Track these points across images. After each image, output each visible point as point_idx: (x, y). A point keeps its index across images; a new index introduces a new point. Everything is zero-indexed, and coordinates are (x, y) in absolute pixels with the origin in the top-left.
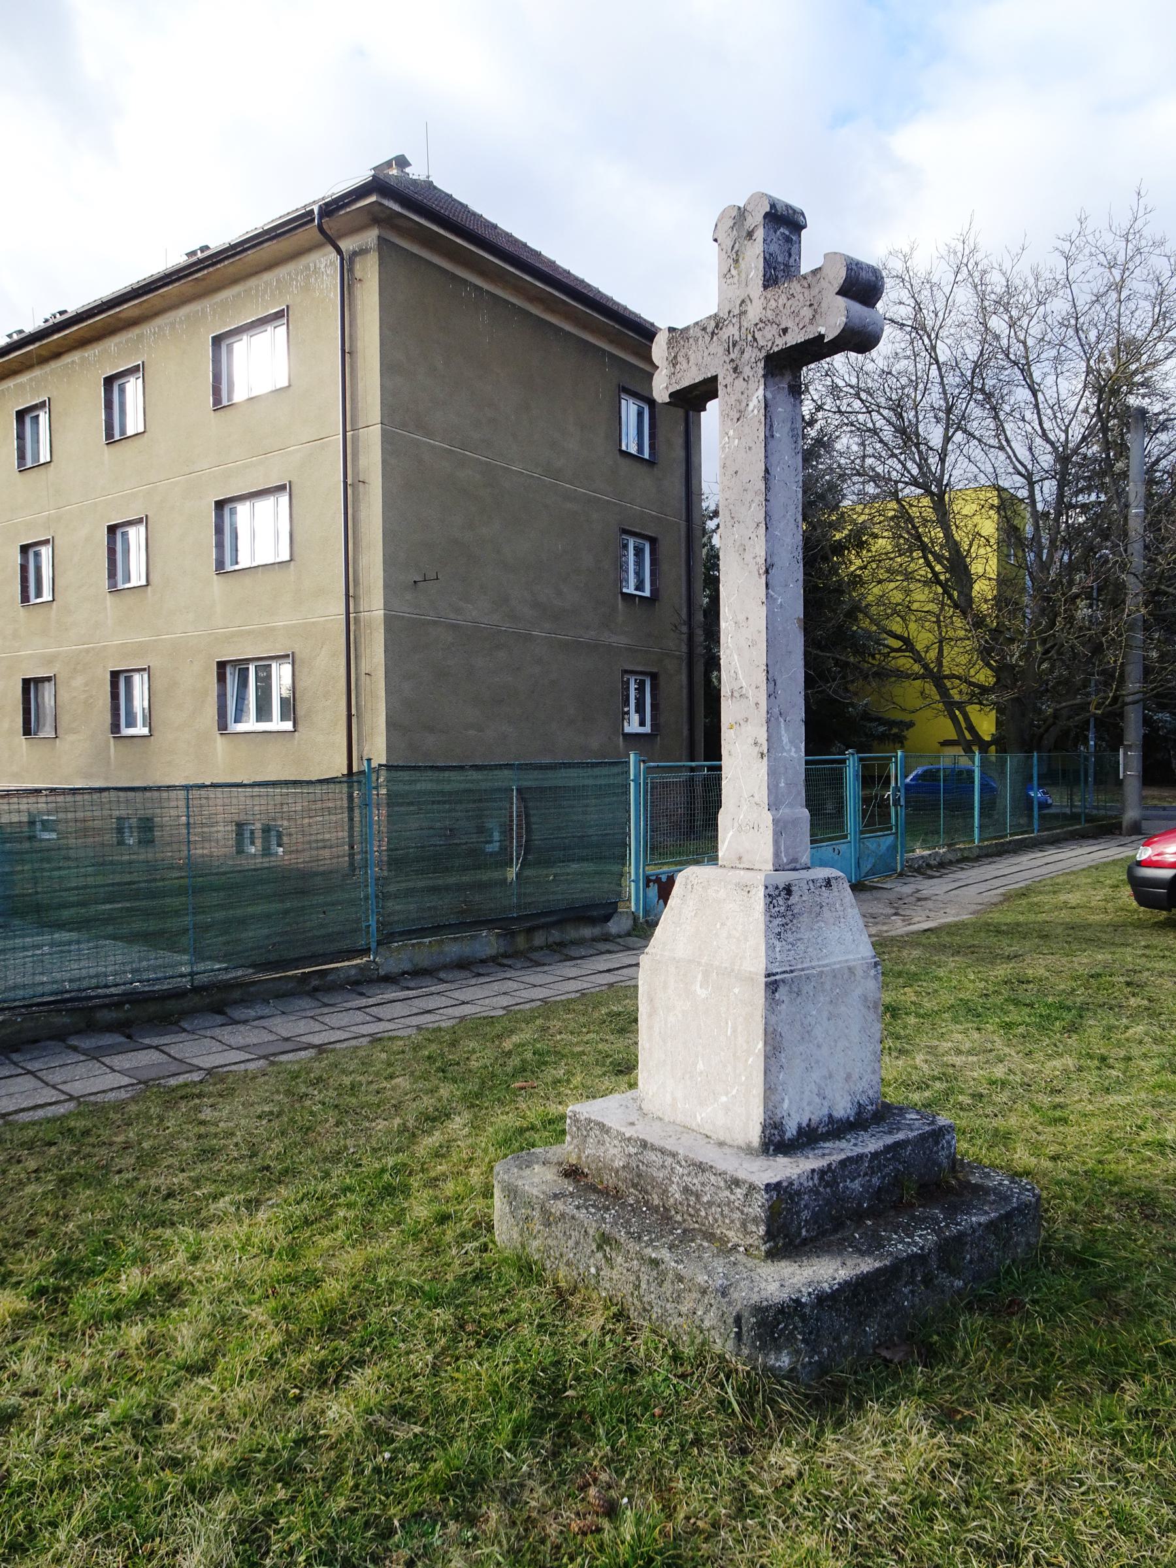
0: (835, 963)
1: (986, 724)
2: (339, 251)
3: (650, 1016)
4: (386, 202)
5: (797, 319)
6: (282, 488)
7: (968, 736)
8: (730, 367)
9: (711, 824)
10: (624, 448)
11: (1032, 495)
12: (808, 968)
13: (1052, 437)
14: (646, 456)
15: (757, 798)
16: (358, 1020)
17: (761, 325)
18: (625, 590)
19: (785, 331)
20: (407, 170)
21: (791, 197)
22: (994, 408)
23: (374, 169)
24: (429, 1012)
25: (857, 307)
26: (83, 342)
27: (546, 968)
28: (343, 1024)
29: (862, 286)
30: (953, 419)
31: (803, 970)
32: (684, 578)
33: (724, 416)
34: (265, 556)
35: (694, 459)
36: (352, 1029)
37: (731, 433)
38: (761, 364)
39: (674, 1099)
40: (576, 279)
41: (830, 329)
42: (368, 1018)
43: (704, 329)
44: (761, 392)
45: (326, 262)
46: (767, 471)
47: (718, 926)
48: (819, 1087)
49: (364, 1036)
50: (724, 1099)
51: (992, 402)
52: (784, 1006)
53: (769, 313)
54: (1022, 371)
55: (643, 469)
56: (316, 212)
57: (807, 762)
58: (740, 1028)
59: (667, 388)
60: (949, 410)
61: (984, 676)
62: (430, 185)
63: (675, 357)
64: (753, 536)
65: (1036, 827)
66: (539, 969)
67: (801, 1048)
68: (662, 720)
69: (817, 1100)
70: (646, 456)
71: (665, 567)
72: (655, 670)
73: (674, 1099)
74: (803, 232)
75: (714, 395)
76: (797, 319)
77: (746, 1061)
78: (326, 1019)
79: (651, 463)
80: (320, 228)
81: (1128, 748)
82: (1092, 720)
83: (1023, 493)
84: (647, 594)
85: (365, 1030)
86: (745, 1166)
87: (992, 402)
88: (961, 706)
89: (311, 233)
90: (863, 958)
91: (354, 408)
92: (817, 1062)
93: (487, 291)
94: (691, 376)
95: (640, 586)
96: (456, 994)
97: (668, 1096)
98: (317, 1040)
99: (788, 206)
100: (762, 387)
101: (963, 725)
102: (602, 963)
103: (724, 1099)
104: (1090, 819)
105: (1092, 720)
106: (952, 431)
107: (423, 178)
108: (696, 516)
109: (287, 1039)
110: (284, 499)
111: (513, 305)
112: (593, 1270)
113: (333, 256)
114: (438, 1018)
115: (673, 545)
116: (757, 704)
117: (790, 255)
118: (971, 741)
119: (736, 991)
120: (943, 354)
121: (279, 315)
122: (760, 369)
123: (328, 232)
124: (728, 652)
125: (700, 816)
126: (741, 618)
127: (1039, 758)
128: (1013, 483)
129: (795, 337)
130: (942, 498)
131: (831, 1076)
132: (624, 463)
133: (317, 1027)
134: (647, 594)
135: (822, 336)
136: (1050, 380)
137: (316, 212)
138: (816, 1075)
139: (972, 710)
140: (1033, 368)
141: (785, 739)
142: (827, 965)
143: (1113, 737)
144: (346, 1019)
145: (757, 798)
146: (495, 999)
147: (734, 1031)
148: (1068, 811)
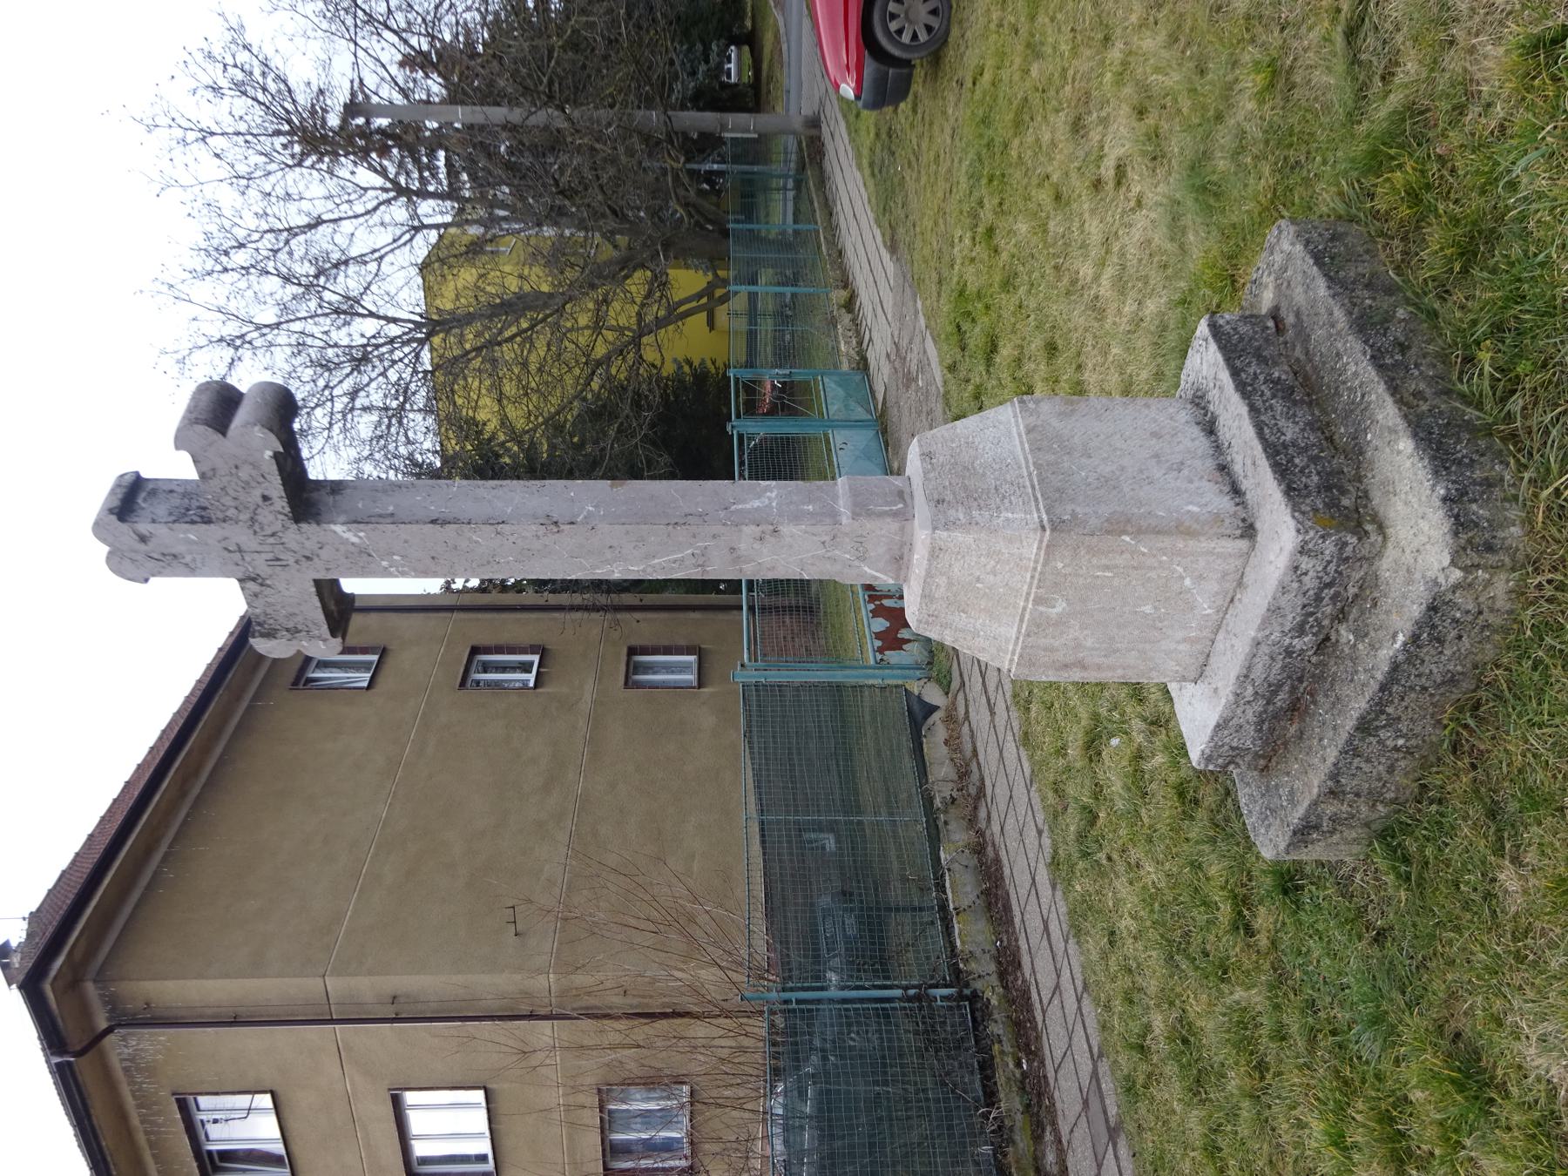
0: (1023, 449)
1: (687, 281)
2: (109, 1030)
3: (1084, 667)
4: (53, 973)
5: (253, 484)
6: (397, 1102)
7: (704, 300)
8: (304, 563)
9: (801, 586)
10: (365, 684)
11: (437, 226)
12: (1031, 481)
13: (370, 206)
14: (375, 658)
16: (1059, 1013)
17: (257, 527)
18: (531, 684)
19: (265, 498)
20: (14, 944)
21: (97, 493)
22: (336, 266)
23: (10, 984)
24: (1046, 928)
25: (242, 415)
26: (96, 1137)
27: (988, 783)
28: (1063, 1032)
29: (219, 406)
30: (348, 309)
31: (1033, 487)
32: (519, 615)
33: (364, 572)
34: (478, 1120)
35: (379, 603)
36: (1070, 1022)
37: (385, 563)
38: (304, 526)
39: (1184, 640)
40: (160, 738)
41: (267, 447)
42: (1056, 1001)
43: (256, 595)
44: (338, 528)
45: (118, 1048)
46: (433, 522)
48: (1171, 469)
49: (1080, 1008)
50: (1188, 582)
51: (328, 268)
52: (1078, 510)
53: (242, 517)
54: (296, 235)
55: (390, 661)
56: (58, 1060)
57: (742, 477)
58: (1104, 561)
59: (325, 640)
60: (337, 311)
61: (637, 283)
62: (34, 918)
63: (288, 630)
64: (512, 539)
65: (811, 227)
66: (989, 791)
67: (1126, 490)
68: (682, 642)
69: (1186, 472)
70: (375, 658)
71: (505, 638)
72: (625, 651)
73: (1184, 640)
74: (144, 475)
75: (335, 583)
76: (253, 484)
78: (1058, 1054)
79: (384, 653)
80: (78, 1054)
81: (724, 127)
82: (688, 166)
83: (433, 236)
84: (536, 658)
85: (1071, 1004)
86: (1272, 558)
87: (328, 268)
88: (672, 308)
89: (85, 1068)
90: (1015, 416)
91: (147, 851)
92: (1141, 471)
93: (170, 846)
94: (314, 611)
95: (526, 667)
96: (1023, 892)
97: (1181, 647)
98: (1086, 1067)
99: (113, 492)
100: (333, 527)
101: (694, 304)
102: (980, 717)
103: (1188, 582)
104: (802, 167)
105: (688, 166)
106: (361, 311)
107: (25, 925)
108: (450, 600)
109: (1086, 1103)
110: (410, 1097)
111: (188, 815)
112: (1401, 742)
113: (111, 1039)
114: (1053, 916)
115: (483, 629)
116: (714, 536)
117: (171, 491)
118: (710, 300)
119: (1060, 565)
120: (269, 316)
121: (183, 1106)
122: (308, 528)
123: (85, 1043)
124: (649, 570)
125: (791, 600)
126: (609, 554)
128: (422, 246)
129: (275, 487)
130: (437, 323)
131: (1156, 456)
132: (384, 683)
133: (1068, 1065)
134: (536, 658)
135: (276, 456)
136: (305, 205)
137: (58, 1060)
138: (1157, 473)
139: (677, 296)
141: (757, 504)
142: (1026, 459)
143: (707, 143)
144: (1058, 1029)
146: (1028, 846)
147: (1107, 568)
148: (791, 194)
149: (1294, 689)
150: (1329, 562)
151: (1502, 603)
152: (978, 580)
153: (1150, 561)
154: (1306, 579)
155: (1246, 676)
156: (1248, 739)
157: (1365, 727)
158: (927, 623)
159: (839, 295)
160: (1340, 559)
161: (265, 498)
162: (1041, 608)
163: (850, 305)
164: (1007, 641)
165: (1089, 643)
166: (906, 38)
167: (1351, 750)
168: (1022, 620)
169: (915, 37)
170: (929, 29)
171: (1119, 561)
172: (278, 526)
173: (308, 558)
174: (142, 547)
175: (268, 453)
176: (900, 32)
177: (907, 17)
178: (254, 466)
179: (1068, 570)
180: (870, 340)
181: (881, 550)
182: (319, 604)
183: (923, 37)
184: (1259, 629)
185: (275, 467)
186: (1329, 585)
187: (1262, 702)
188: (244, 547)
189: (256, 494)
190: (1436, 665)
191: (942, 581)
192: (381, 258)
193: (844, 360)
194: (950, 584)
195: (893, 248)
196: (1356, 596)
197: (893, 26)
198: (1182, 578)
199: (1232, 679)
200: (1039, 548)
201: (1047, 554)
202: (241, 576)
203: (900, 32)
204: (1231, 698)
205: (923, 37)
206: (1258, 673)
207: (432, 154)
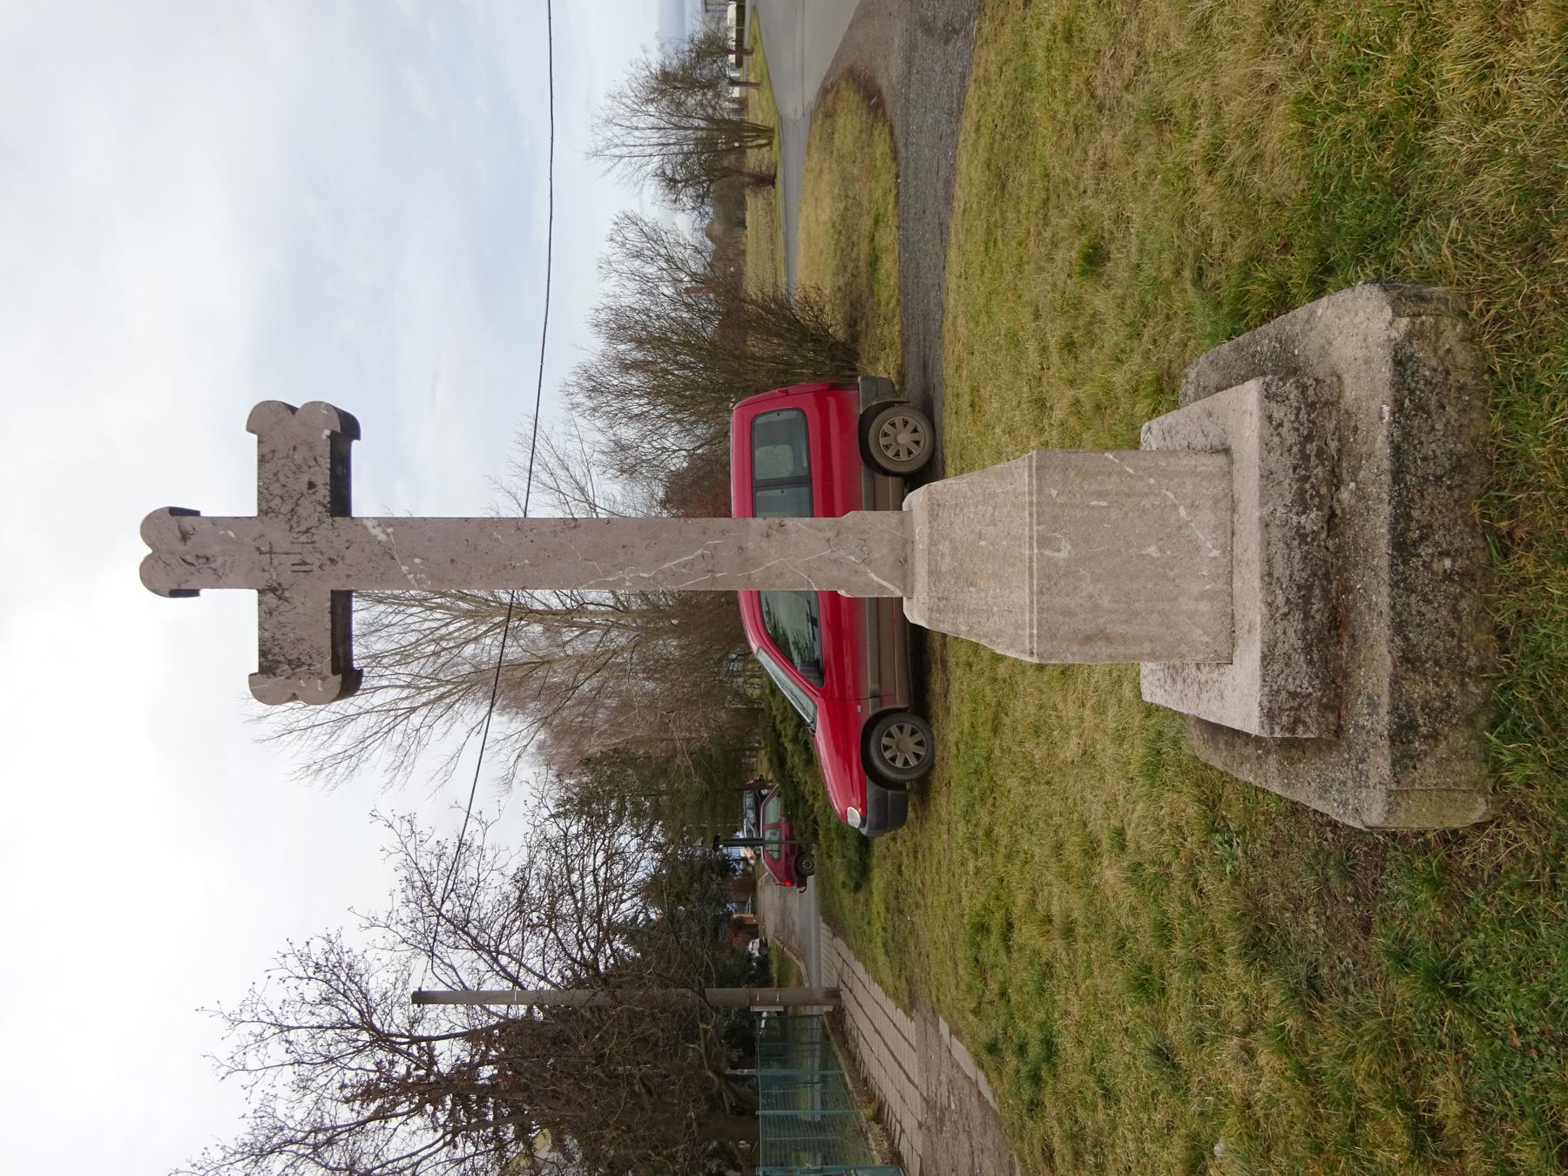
5: (305, 468)
8: (328, 568)
15: (831, 534)
19: (311, 485)
37: (405, 568)
47: (983, 543)
50: (1183, 512)
58: (1095, 487)
64: (531, 537)
65: (836, 1072)
76: (305, 468)
77: (1131, 476)
81: (753, 1002)
103: (1183, 512)
119: (1054, 493)
127: (764, 1108)
135: (333, 434)
140: (340, 1122)
145: (831, 534)
147: (1100, 495)
149: (1326, 592)
150: (1299, 409)
151: (1462, 356)
152: (980, 536)
153: (1140, 485)
154: (1284, 431)
155: (1270, 575)
156: (1302, 679)
157: (1402, 547)
158: (939, 611)
159: (866, 1112)
160: (1307, 405)
161: (311, 485)
162: (1047, 552)
163: (878, 1117)
164: (1022, 609)
165: (1105, 602)
166: (899, 764)
167: (1401, 584)
168: (1031, 576)
169: (906, 762)
170: (917, 756)
171: (1111, 484)
172: (314, 521)
173: (332, 561)
174: (181, 547)
175: (327, 432)
176: (893, 759)
177: (898, 749)
178: (311, 448)
179: (1062, 500)
180: (902, 1131)
181: (885, 550)
182: (329, 626)
183: (913, 762)
184: (1263, 504)
185: (328, 449)
186: (1308, 438)
187: (1299, 615)
188: (276, 549)
189: (305, 479)
190: (1436, 446)
191: (945, 547)
194: (954, 550)
196: (1339, 451)
197: (888, 755)
198: (1175, 507)
199: (1257, 584)
200: (1030, 476)
201: (1039, 479)
202: (262, 585)
203: (893, 759)
204: (1265, 610)
205: (913, 762)
206: (1280, 569)
207: (481, 1101)
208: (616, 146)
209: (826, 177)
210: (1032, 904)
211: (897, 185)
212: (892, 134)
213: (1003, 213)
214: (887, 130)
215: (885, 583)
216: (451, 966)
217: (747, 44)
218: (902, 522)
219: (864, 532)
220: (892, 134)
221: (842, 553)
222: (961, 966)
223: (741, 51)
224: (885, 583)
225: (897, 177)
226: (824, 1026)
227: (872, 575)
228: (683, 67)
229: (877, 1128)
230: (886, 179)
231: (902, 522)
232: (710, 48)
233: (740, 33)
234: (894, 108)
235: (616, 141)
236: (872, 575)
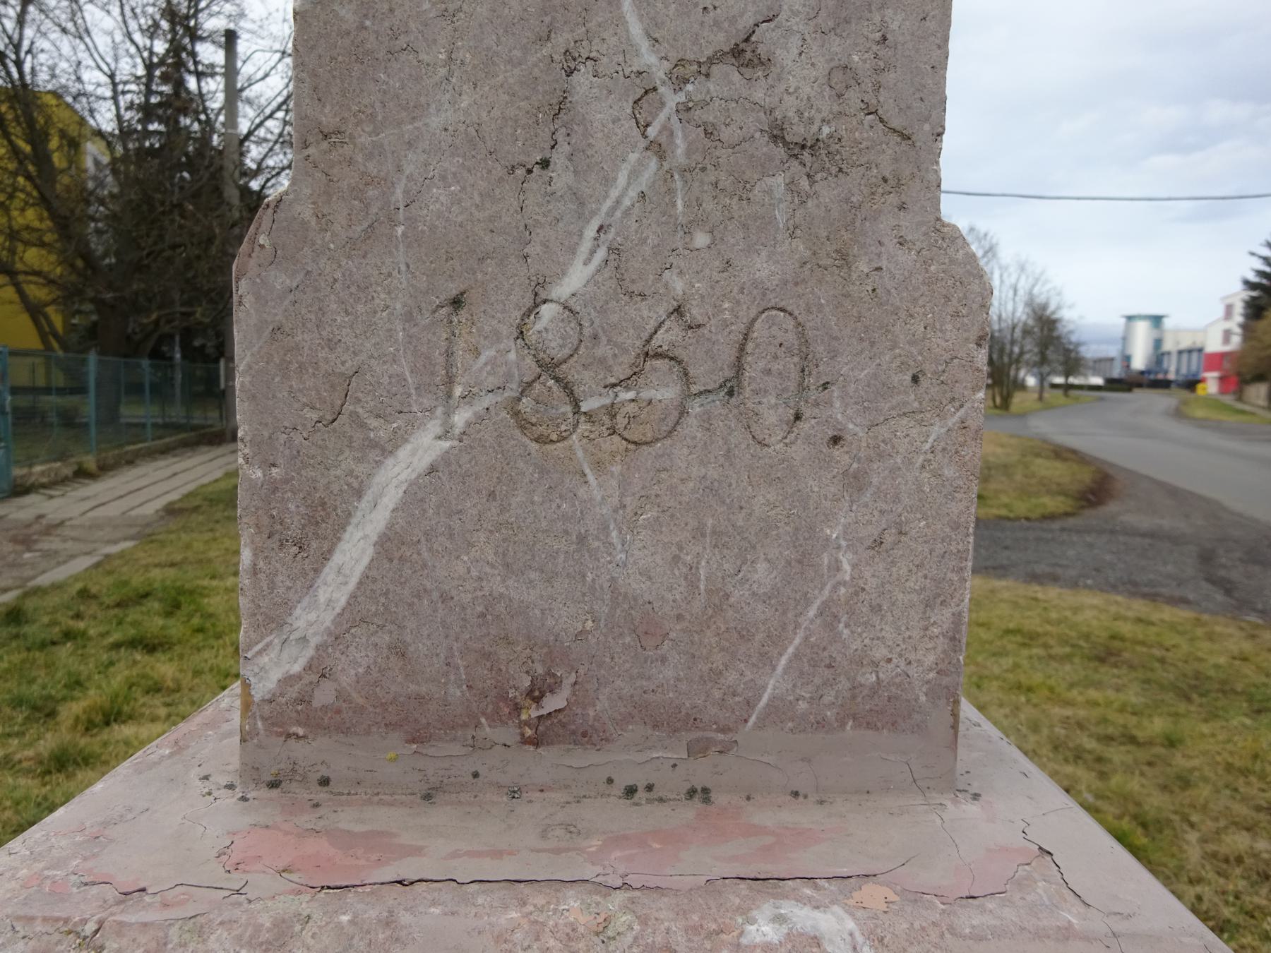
104: (194, 428)
159: (90, 462)
163: (82, 474)
180: (51, 497)
181: (641, 564)
192: (81, 38)
193: (25, 471)
195: (171, 511)
208: (1001, 276)
209: (999, 450)
210: (155, 688)
211: (1018, 519)
212: (1067, 514)
213: (1068, 658)
214: (1069, 510)
215: (354, 552)
216: (266, 75)
217: (1073, 393)
218: (880, 712)
219: (809, 379)
220: (1067, 514)
221: (631, 177)
222: (171, 572)
223: (1068, 387)
224: (354, 552)
225: (1027, 519)
226: (211, 426)
227: (423, 448)
228: (1059, 338)
229: (68, 471)
230: (1021, 508)
231: (880, 712)
232: (1072, 362)
233: (1080, 387)
234: (1092, 517)
235: (1005, 275)
236: (423, 448)
